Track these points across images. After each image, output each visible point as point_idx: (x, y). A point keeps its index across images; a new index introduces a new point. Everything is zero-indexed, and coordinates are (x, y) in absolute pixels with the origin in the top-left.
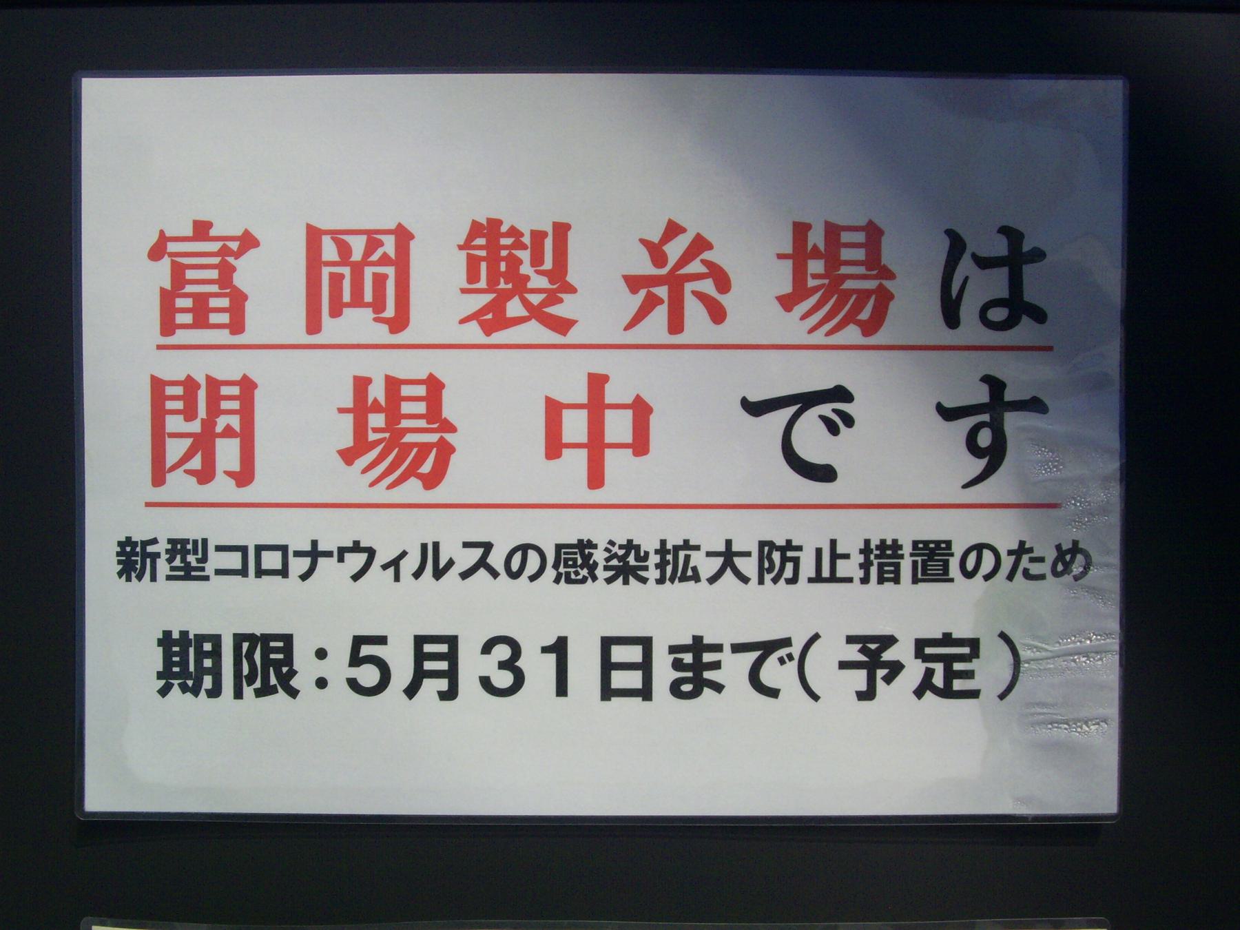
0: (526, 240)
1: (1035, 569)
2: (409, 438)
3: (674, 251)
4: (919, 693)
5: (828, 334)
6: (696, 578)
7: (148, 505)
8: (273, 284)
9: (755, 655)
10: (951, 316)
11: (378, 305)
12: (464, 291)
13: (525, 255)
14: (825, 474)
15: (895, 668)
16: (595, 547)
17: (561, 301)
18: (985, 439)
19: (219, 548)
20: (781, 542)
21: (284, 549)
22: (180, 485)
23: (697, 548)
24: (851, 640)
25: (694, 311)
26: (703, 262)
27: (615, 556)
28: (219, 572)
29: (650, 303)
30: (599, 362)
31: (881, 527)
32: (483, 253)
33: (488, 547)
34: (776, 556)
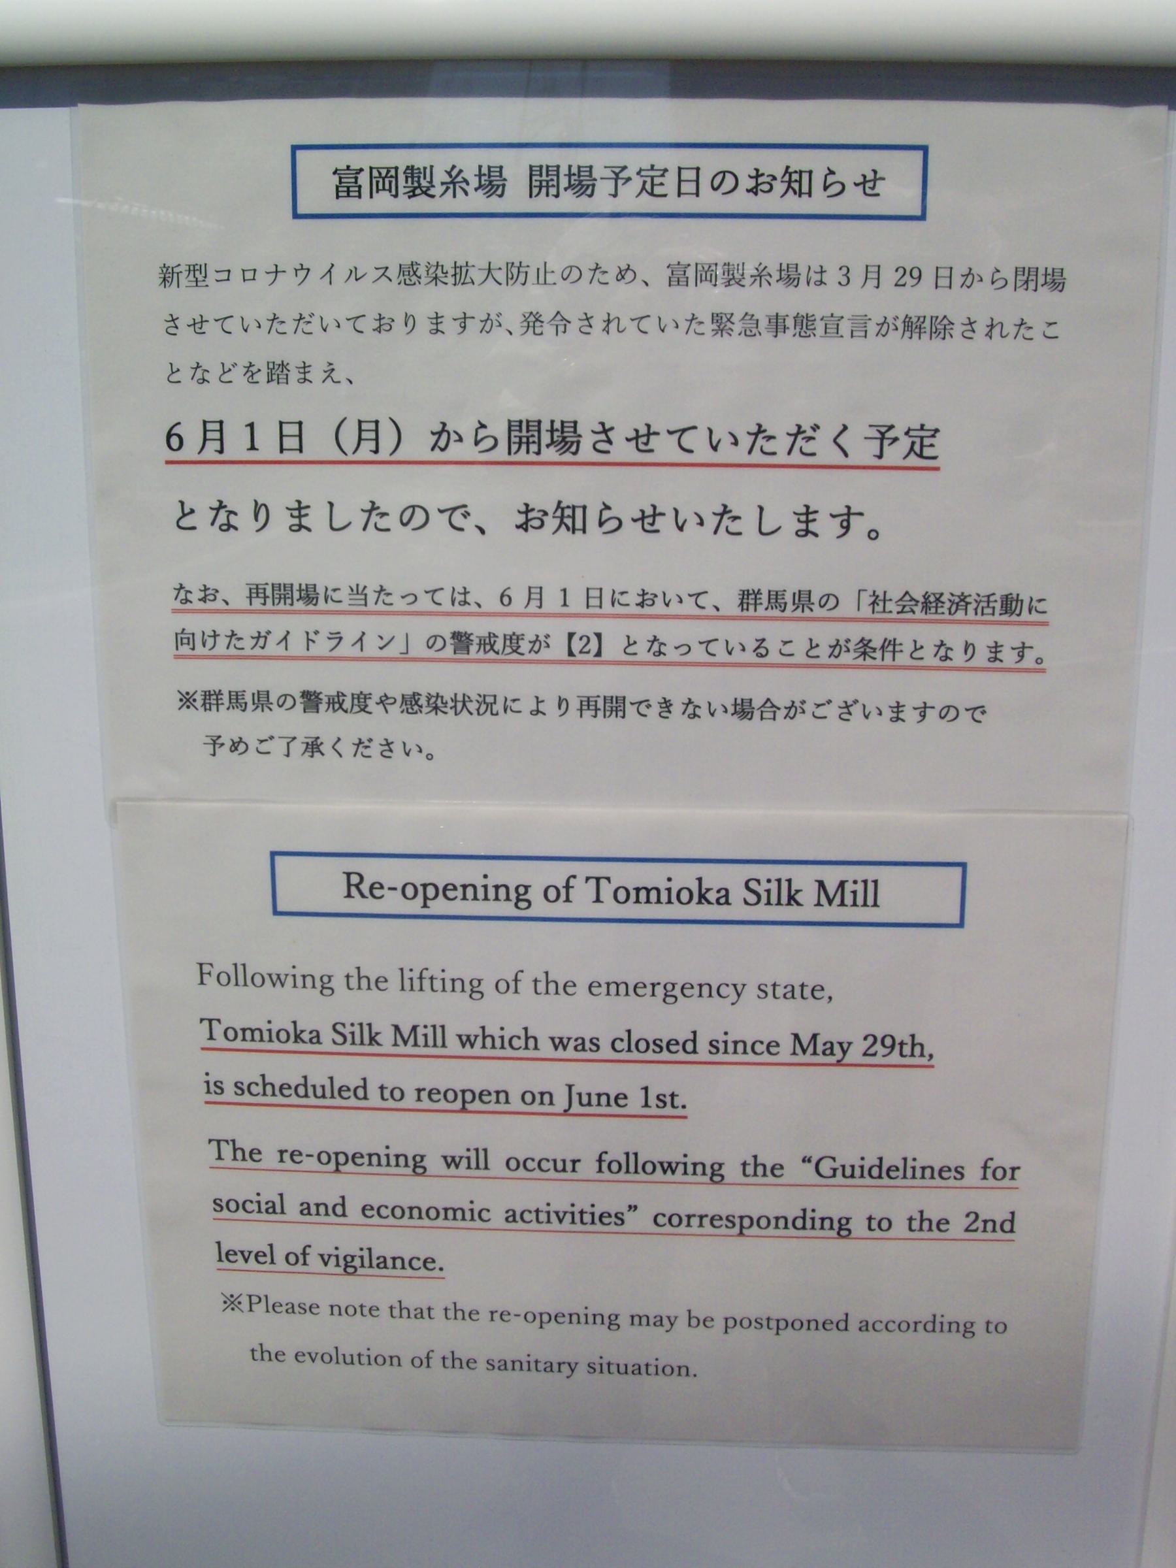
3: (454, 173)
7: (203, 1049)
11: (390, 190)
18: (845, 524)
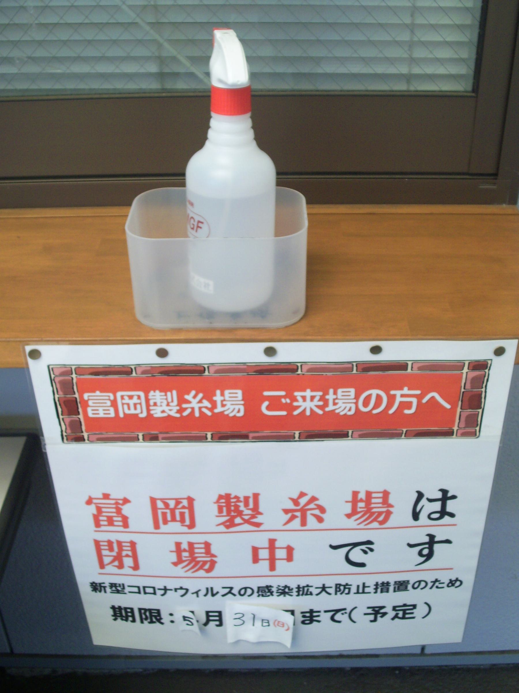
0: (242, 499)
1: (440, 586)
2: (199, 559)
3: (303, 501)
4: (393, 619)
5: (366, 525)
6: (311, 594)
8: (139, 515)
9: (333, 613)
10: (416, 516)
11: (182, 520)
12: (217, 516)
13: (242, 505)
14: (363, 565)
15: (384, 614)
16: (272, 587)
17: (257, 517)
19: (129, 586)
20: (344, 583)
21: (154, 588)
22: (110, 569)
23: (312, 586)
24: (368, 608)
25: (311, 521)
26: (316, 505)
27: (280, 589)
28: (130, 592)
29: (293, 518)
30: (272, 535)
31: (381, 579)
32: (224, 504)
33: (231, 588)
34: (342, 588)
